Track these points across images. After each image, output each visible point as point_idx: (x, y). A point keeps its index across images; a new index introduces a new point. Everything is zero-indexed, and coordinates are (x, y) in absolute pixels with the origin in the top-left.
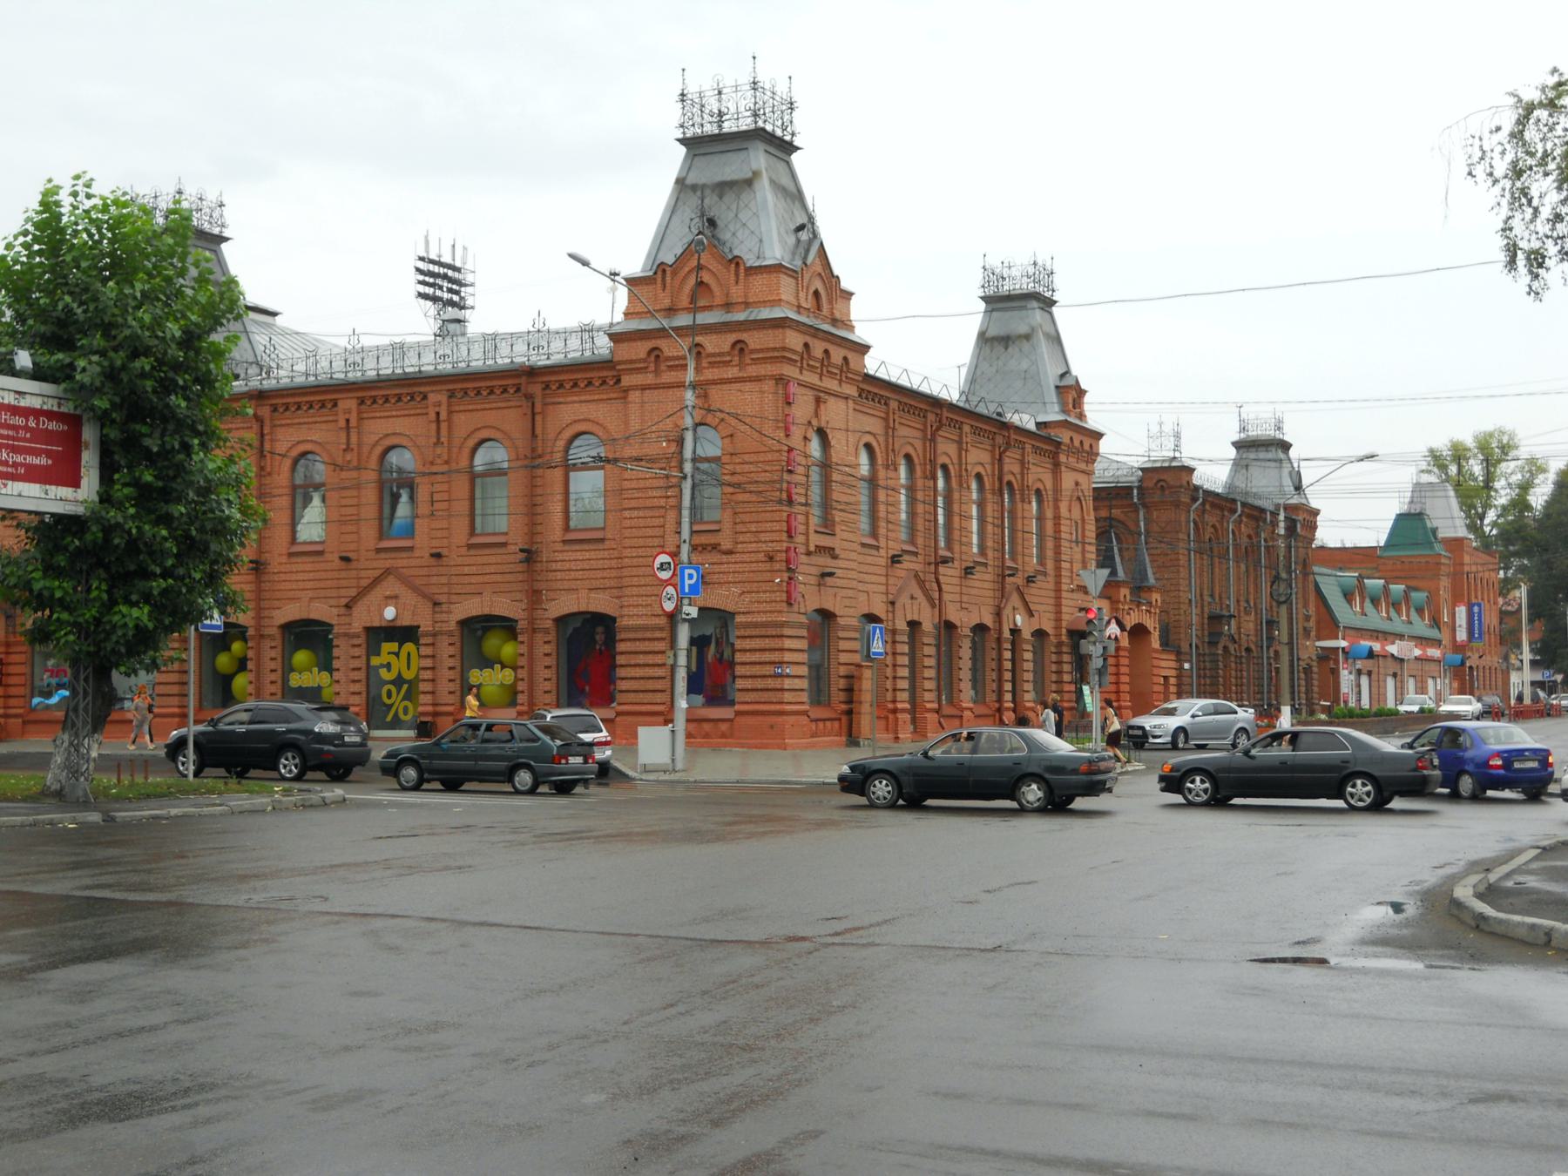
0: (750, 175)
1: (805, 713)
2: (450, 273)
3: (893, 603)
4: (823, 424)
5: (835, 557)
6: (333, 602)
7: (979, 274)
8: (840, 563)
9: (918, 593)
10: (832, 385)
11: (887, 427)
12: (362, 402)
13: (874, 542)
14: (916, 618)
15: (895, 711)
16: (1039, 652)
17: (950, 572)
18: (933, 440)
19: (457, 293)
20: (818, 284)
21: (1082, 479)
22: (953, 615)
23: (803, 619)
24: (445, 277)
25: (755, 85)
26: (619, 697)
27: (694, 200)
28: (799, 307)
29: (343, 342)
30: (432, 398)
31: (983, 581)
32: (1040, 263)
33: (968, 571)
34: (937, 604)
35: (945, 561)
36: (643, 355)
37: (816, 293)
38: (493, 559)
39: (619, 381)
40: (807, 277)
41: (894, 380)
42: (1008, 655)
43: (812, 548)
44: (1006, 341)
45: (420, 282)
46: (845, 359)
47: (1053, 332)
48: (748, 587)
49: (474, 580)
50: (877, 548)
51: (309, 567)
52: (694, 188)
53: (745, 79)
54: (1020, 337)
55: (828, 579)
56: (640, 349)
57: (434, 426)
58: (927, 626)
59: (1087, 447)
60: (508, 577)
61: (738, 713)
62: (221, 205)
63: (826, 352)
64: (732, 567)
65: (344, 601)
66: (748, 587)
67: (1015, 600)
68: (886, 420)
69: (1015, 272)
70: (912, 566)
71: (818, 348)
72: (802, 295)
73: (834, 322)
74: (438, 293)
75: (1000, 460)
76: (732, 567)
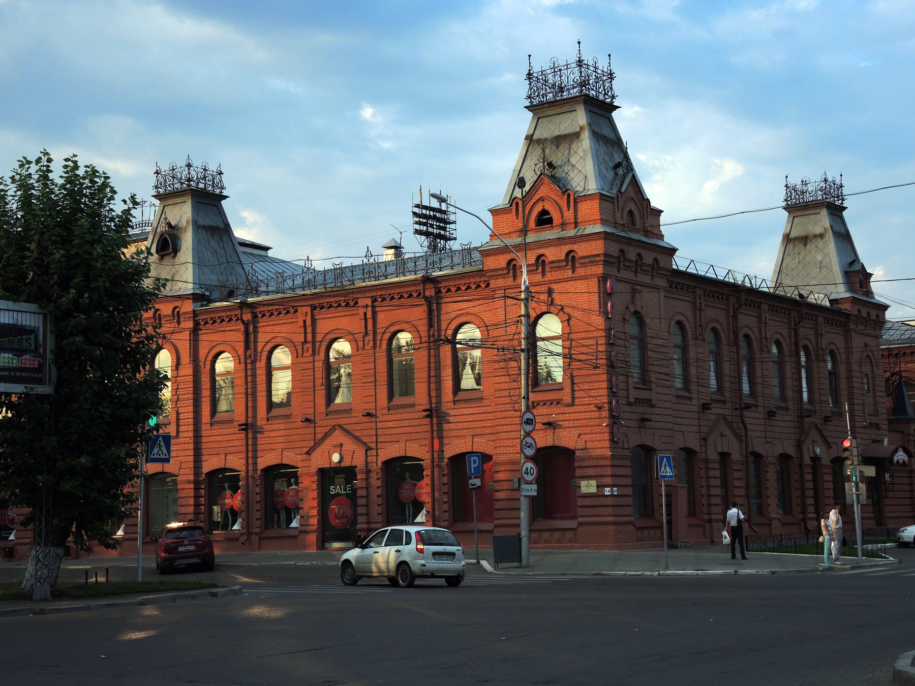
0: (578, 129)
1: (632, 523)
2: (438, 215)
3: (705, 439)
4: (639, 309)
5: (653, 406)
6: (298, 451)
7: (783, 191)
8: (657, 411)
9: (727, 432)
10: (647, 279)
11: (695, 309)
12: (314, 308)
13: (687, 394)
14: (725, 450)
15: (710, 521)
16: (783, 476)
17: (754, 415)
18: (735, 317)
19: (444, 229)
20: (632, 206)
21: (871, 342)
22: (760, 448)
23: (628, 453)
24: (434, 218)
25: (580, 63)
26: (497, 514)
27: (537, 152)
28: (616, 223)
29: (302, 263)
30: (362, 302)
31: (785, 422)
32: (830, 179)
33: (771, 414)
34: (743, 438)
35: (748, 407)
36: (504, 265)
37: (630, 212)
38: (406, 416)
39: (488, 285)
40: (621, 201)
41: (702, 273)
42: (809, 477)
43: (632, 400)
44: (805, 240)
45: (416, 223)
46: (655, 259)
47: (843, 230)
48: (584, 430)
49: (394, 431)
50: (690, 399)
51: (282, 426)
52: (539, 141)
53: (573, 59)
54: (815, 236)
55: (647, 423)
56: (501, 261)
57: (363, 321)
58: (736, 455)
59: (873, 317)
60: (417, 429)
61: (580, 524)
62: (221, 173)
63: (639, 255)
64: (572, 416)
65: (306, 450)
66: (584, 430)
67: (814, 435)
68: (694, 303)
69: (810, 188)
70: (721, 411)
71: (632, 254)
72: (618, 215)
73: (647, 233)
74: (430, 230)
75: (796, 330)
76: (572, 416)
